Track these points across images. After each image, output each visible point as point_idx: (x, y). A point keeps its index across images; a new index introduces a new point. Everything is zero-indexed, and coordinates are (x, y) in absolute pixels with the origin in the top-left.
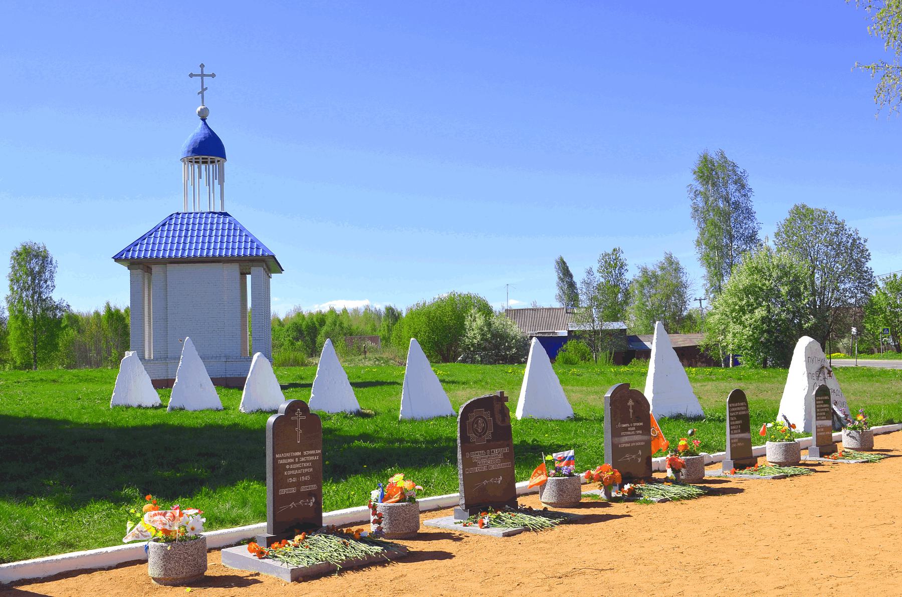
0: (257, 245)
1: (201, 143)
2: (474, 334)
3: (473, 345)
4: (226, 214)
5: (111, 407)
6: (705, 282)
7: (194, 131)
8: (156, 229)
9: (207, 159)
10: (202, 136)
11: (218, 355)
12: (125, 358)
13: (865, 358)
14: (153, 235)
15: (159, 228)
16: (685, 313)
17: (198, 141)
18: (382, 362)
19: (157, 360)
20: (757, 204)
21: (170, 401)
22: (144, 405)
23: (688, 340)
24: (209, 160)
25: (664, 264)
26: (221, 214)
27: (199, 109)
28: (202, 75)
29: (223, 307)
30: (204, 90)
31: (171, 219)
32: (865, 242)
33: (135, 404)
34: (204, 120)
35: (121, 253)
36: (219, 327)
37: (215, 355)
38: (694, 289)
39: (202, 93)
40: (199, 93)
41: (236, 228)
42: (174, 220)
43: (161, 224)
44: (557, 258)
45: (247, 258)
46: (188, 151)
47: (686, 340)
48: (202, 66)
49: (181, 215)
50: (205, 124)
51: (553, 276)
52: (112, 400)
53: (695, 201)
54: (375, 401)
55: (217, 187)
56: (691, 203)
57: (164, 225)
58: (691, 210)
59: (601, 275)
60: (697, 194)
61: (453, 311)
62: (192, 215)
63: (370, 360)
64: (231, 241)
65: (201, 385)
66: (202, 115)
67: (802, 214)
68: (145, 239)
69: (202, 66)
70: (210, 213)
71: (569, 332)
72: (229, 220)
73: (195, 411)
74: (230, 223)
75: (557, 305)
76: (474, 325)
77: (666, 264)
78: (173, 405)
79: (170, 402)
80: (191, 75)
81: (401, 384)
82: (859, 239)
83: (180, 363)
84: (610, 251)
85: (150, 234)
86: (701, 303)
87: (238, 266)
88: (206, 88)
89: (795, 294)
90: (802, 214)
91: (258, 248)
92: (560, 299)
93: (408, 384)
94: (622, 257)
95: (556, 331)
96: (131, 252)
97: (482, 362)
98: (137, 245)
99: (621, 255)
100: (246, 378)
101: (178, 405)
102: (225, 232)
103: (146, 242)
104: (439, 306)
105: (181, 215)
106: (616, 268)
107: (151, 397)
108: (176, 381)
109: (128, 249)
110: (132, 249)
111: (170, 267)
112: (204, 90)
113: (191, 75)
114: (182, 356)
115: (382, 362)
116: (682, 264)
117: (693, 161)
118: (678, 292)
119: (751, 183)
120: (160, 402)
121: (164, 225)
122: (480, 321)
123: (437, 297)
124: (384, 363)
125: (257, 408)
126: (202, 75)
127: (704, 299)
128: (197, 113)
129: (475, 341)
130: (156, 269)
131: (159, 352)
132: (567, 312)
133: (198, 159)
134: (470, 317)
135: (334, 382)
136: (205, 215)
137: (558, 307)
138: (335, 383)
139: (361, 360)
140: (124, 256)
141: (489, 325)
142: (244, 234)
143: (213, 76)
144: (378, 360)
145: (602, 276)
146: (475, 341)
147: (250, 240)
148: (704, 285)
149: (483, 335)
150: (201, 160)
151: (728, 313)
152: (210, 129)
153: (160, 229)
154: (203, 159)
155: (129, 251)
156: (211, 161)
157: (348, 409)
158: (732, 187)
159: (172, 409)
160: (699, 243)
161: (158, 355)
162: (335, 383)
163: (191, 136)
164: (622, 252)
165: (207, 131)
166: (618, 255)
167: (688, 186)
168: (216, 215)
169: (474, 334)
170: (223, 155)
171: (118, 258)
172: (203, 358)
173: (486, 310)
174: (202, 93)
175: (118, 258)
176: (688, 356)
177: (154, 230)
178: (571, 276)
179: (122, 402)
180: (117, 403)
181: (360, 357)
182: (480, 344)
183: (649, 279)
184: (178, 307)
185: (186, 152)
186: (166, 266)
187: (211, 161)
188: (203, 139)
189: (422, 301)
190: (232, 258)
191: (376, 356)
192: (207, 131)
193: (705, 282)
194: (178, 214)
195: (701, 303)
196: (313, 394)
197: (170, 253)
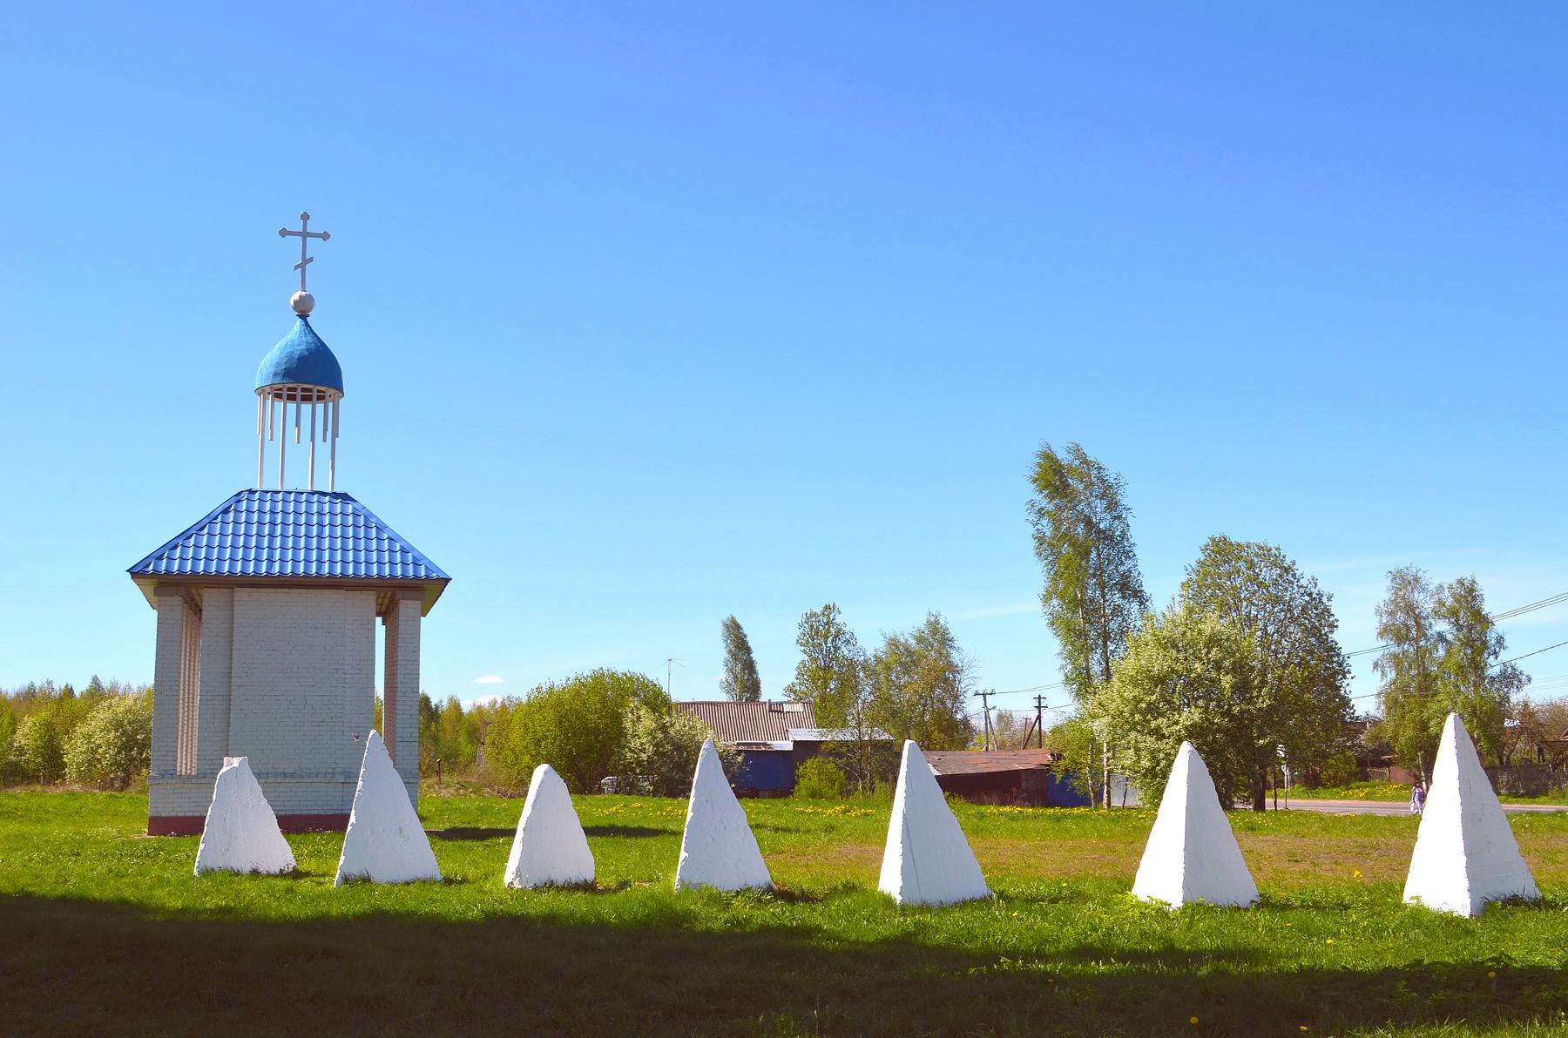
0: (413, 557)
1: (301, 359)
2: (642, 744)
3: (640, 763)
4: (345, 497)
5: (196, 872)
6: (1064, 663)
7: (288, 338)
8: (211, 519)
9: (310, 390)
10: (303, 347)
11: (330, 771)
12: (224, 770)
13: (1527, 804)
14: (206, 530)
15: (216, 518)
16: (959, 716)
17: (296, 357)
18: (470, 790)
19: (205, 777)
20: (1141, 533)
21: (341, 862)
22: (263, 869)
23: (994, 761)
24: (315, 394)
25: (923, 632)
26: (335, 495)
27: (296, 296)
28: (305, 235)
29: (343, 676)
30: (306, 261)
31: (239, 501)
32: (1329, 600)
33: (246, 868)
34: (303, 316)
35: (146, 562)
36: (332, 715)
37: (324, 771)
38: (975, 675)
39: (302, 266)
40: (296, 267)
41: (368, 523)
42: (244, 503)
43: (221, 509)
44: (725, 616)
45: (372, 581)
46: (276, 374)
47: (991, 762)
48: (305, 217)
49: (257, 496)
50: (307, 324)
51: (718, 651)
52: (197, 859)
53: (1039, 527)
54: (466, 860)
55: (323, 449)
56: (1032, 530)
57: (226, 511)
58: (1034, 543)
59: (802, 648)
60: (1041, 513)
61: (603, 702)
62: (280, 496)
63: (448, 786)
64: (215, 557)
65: (401, 831)
66: (301, 308)
67: (1222, 551)
68: (190, 537)
69: (305, 217)
70: (313, 493)
71: (796, 743)
72: (354, 508)
73: (393, 884)
74: (356, 515)
75: (723, 697)
76: (640, 728)
77: (926, 632)
78: (347, 871)
79: (340, 864)
80: (283, 233)
81: (677, 834)
82: (1320, 595)
83: (360, 783)
84: (819, 609)
85: (198, 528)
86: (985, 699)
87: (375, 597)
88: (296, 267)
89: (1242, 688)
90: (1222, 551)
91: (416, 564)
92: (728, 688)
93: (908, 835)
94: (839, 619)
95: (769, 742)
96: (165, 561)
97: (655, 794)
98: (175, 547)
99: (837, 617)
100: (204, 818)
101: (355, 871)
102: (214, 539)
103: (192, 543)
104: (578, 693)
105: (257, 494)
106: (828, 638)
107: (278, 852)
108: (352, 819)
109: (157, 554)
110: (165, 556)
111: (241, 594)
112: (306, 261)
113: (283, 233)
114: (362, 770)
115: (470, 790)
116: (953, 633)
117: (1028, 464)
118: (946, 680)
119: (1126, 498)
120: (294, 863)
121: (226, 511)
122: (648, 722)
123: (573, 677)
124: (474, 792)
125: (545, 878)
126: (305, 235)
127: (991, 694)
128: (292, 303)
129: (644, 756)
130: (211, 600)
131: (210, 762)
132: (771, 711)
133: (295, 389)
134: (630, 715)
135: (722, 827)
136: (304, 496)
137: (725, 700)
138: (725, 828)
139: (434, 786)
140: (151, 567)
141: (664, 729)
142: (386, 536)
143: (325, 236)
144: (462, 786)
145: (804, 651)
146: (644, 756)
147: (398, 548)
148: (1062, 667)
149: (656, 745)
150: (299, 393)
151: (1127, 715)
152: (318, 339)
153: (219, 520)
154: (303, 390)
155: (160, 558)
156: (302, 395)
157: (753, 883)
158: (1100, 505)
159: (346, 879)
160: (1047, 599)
161: (207, 767)
162: (725, 828)
163: (280, 344)
164: (839, 612)
165: (310, 338)
166: (831, 616)
167: (1027, 503)
168: (327, 498)
169: (642, 744)
170: (340, 388)
171: (127, 571)
172: (258, 776)
173: (657, 701)
174: (302, 266)
175: (127, 571)
176: (956, 786)
177: (207, 521)
178: (748, 650)
179: (217, 862)
180: (210, 864)
181: (430, 781)
182: (653, 762)
183: (902, 657)
184: (253, 674)
185: (271, 375)
186: (233, 592)
187: (302, 395)
188: (306, 354)
189: (548, 684)
190: (367, 581)
191: (460, 780)
192: (310, 338)
193: (1064, 663)
194: (251, 492)
195: (985, 699)
196: (686, 851)
197: (231, 565)
